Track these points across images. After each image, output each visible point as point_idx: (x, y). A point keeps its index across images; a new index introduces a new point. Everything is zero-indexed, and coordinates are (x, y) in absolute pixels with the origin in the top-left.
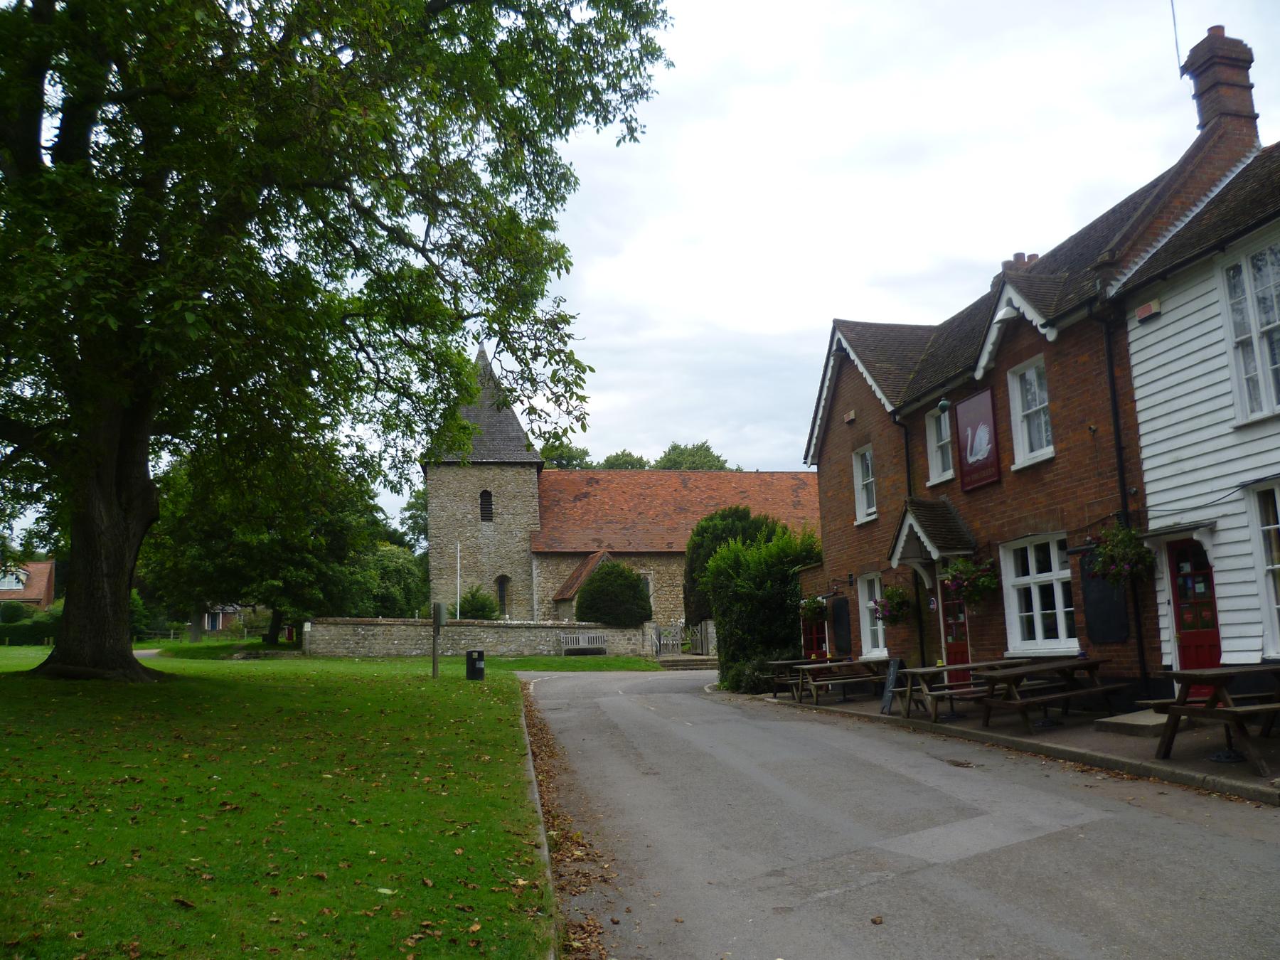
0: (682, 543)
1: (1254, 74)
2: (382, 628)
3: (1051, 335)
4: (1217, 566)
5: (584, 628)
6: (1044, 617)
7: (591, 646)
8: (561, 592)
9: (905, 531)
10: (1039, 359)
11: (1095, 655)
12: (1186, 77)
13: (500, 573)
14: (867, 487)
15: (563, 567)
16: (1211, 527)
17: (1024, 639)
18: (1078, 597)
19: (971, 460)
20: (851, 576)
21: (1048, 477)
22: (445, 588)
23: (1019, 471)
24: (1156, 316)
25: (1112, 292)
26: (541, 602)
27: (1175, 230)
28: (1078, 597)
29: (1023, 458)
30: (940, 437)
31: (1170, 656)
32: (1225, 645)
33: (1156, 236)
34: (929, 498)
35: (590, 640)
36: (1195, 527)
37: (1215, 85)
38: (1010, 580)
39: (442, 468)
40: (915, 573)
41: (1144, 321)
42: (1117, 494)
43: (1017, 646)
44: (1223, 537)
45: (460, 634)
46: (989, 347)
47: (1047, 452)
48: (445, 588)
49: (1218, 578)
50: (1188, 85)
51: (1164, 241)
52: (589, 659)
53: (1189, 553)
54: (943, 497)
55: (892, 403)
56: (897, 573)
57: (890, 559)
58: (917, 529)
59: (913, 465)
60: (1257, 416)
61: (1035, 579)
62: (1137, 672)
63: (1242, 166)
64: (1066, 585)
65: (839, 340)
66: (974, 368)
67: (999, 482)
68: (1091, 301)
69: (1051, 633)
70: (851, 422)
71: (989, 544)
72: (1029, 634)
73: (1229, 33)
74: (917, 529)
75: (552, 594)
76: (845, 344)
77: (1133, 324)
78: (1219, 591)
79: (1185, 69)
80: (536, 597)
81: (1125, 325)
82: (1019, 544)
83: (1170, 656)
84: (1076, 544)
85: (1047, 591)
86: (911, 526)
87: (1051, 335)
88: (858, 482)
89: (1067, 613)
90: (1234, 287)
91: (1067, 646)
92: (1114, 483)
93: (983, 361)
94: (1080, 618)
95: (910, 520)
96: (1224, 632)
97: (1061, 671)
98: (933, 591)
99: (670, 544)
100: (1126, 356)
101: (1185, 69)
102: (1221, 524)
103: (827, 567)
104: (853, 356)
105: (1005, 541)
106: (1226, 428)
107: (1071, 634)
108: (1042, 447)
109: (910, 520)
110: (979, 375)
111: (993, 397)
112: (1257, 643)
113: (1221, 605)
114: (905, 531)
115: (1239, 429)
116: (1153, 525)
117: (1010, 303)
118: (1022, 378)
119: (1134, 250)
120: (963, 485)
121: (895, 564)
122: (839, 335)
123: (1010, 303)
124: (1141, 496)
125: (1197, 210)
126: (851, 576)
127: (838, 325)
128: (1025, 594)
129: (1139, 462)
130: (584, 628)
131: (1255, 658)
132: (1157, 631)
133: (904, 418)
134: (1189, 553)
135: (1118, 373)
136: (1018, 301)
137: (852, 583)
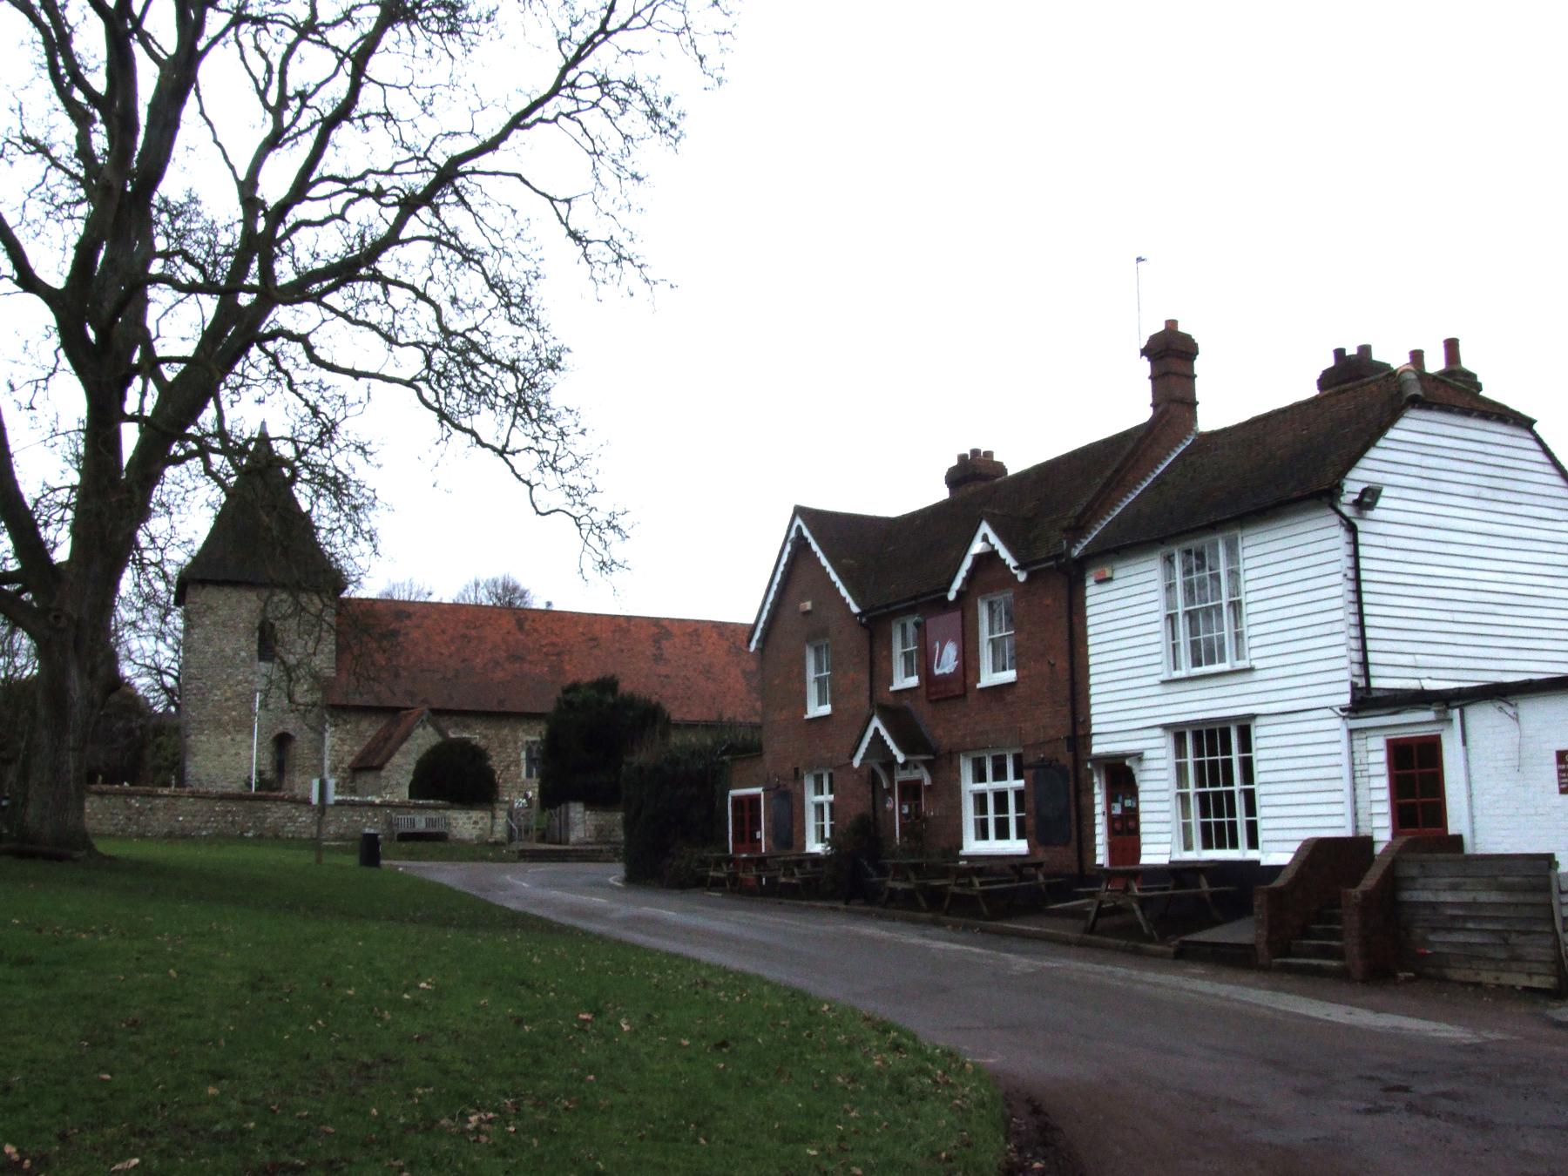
0: (548, 705)
1: (1199, 365)
2: (165, 801)
3: (1022, 577)
4: (1142, 787)
5: (422, 807)
6: (997, 821)
7: (432, 830)
8: (361, 758)
9: (870, 733)
10: (1009, 594)
11: (1042, 855)
12: (1145, 358)
13: (281, 729)
14: (819, 681)
15: (364, 725)
16: (1138, 756)
17: (977, 838)
18: (1030, 803)
19: (937, 672)
20: (796, 770)
21: (1009, 698)
22: (207, 746)
23: (982, 690)
24: (1110, 579)
25: (1076, 553)
26: (334, 770)
27: (1127, 501)
28: (1030, 803)
29: (990, 677)
30: (904, 645)
31: (1102, 857)
32: (1144, 849)
33: (1113, 506)
34: (891, 702)
35: (429, 822)
36: (1124, 756)
37: (1166, 374)
38: (969, 786)
39: (209, 588)
40: (873, 771)
41: (1100, 582)
42: (1068, 721)
43: (972, 846)
44: (1146, 765)
45: (266, 810)
46: (962, 573)
47: (1009, 676)
48: (207, 746)
49: (1142, 796)
50: (1145, 366)
51: (1118, 510)
52: (420, 845)
53: (1121, 775)
54: (906, 702)
55: (858, 604)
56: (856, 771)
57: (852, 756)
58: (883, 732)
59: (878, 672)
60: (1177, 674)
61: (990, 786)
62: (1075, 870)
63: (1183, 447)
64: (1019, 794)
65: (799, 528)
66: (947, 589)
67: (964, 696)
68: (1057, 557)
69: (1002, 833)
70: (807, 613)
71: (950, 752)
72: (983, 834)
73: (1182, 328)
74: (883, 732)
75: (349, 760)
76: (806, 533)
77: (1090, 582)
78: (1142, 807)
79: (1144, 352)
80: (327, 763)
81: (1084, 581)
82: (977, 755)
83: (1102, 857)
84: (1030, 759)
85: (1001, 797)
86: (876, 730)
87: (1022, 577)
88: (811, 674)
89: (1018, 819)
90: (1169, 560)
91: (1017, 846)
92: (1066, 710)
93: (957, 584)
94: (1030, 823)
95: (876, 722)
96: (1144, 839)
97: (1013, 867)
98: (890, 791)
99: (501, 702)
100: (1083, 607)
101: (1144, 352)
102: (1147, 754)
103: (768, 758)
104: (815, 547)
105: (966, 751)
106: (1155, 680)
107: (1020, 836)
108: (1004, 669)
109: (876, 722)
110: (952, 596)
111: (963, 617)
112: (1167, 848)
113: (1143, 817)
114: (870, 733)
115: (1164, 682)
116: (1096, 750)
117: (985, 538)
118: (991, 605)
119: (1097, 517)
120: (928, 694)
121: (856, 763)
122: (799, 521)
123: (985, 538)
124: (1087, 723)
125: (1145, 484)
126: (796, 770)
127: (800, 511)
128: (981, 799)
129: (1087, 697)
130: (422, 807)
131: (1164, 860)
132: (1093, 836)
133: (869, 619)
134: (1121, 775)
135: (1075, 618)
136: (993, 539)
137: (798, 776)
